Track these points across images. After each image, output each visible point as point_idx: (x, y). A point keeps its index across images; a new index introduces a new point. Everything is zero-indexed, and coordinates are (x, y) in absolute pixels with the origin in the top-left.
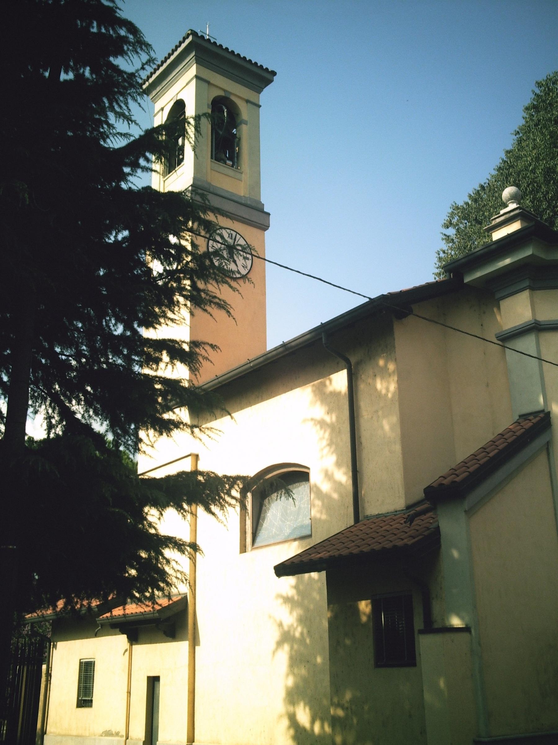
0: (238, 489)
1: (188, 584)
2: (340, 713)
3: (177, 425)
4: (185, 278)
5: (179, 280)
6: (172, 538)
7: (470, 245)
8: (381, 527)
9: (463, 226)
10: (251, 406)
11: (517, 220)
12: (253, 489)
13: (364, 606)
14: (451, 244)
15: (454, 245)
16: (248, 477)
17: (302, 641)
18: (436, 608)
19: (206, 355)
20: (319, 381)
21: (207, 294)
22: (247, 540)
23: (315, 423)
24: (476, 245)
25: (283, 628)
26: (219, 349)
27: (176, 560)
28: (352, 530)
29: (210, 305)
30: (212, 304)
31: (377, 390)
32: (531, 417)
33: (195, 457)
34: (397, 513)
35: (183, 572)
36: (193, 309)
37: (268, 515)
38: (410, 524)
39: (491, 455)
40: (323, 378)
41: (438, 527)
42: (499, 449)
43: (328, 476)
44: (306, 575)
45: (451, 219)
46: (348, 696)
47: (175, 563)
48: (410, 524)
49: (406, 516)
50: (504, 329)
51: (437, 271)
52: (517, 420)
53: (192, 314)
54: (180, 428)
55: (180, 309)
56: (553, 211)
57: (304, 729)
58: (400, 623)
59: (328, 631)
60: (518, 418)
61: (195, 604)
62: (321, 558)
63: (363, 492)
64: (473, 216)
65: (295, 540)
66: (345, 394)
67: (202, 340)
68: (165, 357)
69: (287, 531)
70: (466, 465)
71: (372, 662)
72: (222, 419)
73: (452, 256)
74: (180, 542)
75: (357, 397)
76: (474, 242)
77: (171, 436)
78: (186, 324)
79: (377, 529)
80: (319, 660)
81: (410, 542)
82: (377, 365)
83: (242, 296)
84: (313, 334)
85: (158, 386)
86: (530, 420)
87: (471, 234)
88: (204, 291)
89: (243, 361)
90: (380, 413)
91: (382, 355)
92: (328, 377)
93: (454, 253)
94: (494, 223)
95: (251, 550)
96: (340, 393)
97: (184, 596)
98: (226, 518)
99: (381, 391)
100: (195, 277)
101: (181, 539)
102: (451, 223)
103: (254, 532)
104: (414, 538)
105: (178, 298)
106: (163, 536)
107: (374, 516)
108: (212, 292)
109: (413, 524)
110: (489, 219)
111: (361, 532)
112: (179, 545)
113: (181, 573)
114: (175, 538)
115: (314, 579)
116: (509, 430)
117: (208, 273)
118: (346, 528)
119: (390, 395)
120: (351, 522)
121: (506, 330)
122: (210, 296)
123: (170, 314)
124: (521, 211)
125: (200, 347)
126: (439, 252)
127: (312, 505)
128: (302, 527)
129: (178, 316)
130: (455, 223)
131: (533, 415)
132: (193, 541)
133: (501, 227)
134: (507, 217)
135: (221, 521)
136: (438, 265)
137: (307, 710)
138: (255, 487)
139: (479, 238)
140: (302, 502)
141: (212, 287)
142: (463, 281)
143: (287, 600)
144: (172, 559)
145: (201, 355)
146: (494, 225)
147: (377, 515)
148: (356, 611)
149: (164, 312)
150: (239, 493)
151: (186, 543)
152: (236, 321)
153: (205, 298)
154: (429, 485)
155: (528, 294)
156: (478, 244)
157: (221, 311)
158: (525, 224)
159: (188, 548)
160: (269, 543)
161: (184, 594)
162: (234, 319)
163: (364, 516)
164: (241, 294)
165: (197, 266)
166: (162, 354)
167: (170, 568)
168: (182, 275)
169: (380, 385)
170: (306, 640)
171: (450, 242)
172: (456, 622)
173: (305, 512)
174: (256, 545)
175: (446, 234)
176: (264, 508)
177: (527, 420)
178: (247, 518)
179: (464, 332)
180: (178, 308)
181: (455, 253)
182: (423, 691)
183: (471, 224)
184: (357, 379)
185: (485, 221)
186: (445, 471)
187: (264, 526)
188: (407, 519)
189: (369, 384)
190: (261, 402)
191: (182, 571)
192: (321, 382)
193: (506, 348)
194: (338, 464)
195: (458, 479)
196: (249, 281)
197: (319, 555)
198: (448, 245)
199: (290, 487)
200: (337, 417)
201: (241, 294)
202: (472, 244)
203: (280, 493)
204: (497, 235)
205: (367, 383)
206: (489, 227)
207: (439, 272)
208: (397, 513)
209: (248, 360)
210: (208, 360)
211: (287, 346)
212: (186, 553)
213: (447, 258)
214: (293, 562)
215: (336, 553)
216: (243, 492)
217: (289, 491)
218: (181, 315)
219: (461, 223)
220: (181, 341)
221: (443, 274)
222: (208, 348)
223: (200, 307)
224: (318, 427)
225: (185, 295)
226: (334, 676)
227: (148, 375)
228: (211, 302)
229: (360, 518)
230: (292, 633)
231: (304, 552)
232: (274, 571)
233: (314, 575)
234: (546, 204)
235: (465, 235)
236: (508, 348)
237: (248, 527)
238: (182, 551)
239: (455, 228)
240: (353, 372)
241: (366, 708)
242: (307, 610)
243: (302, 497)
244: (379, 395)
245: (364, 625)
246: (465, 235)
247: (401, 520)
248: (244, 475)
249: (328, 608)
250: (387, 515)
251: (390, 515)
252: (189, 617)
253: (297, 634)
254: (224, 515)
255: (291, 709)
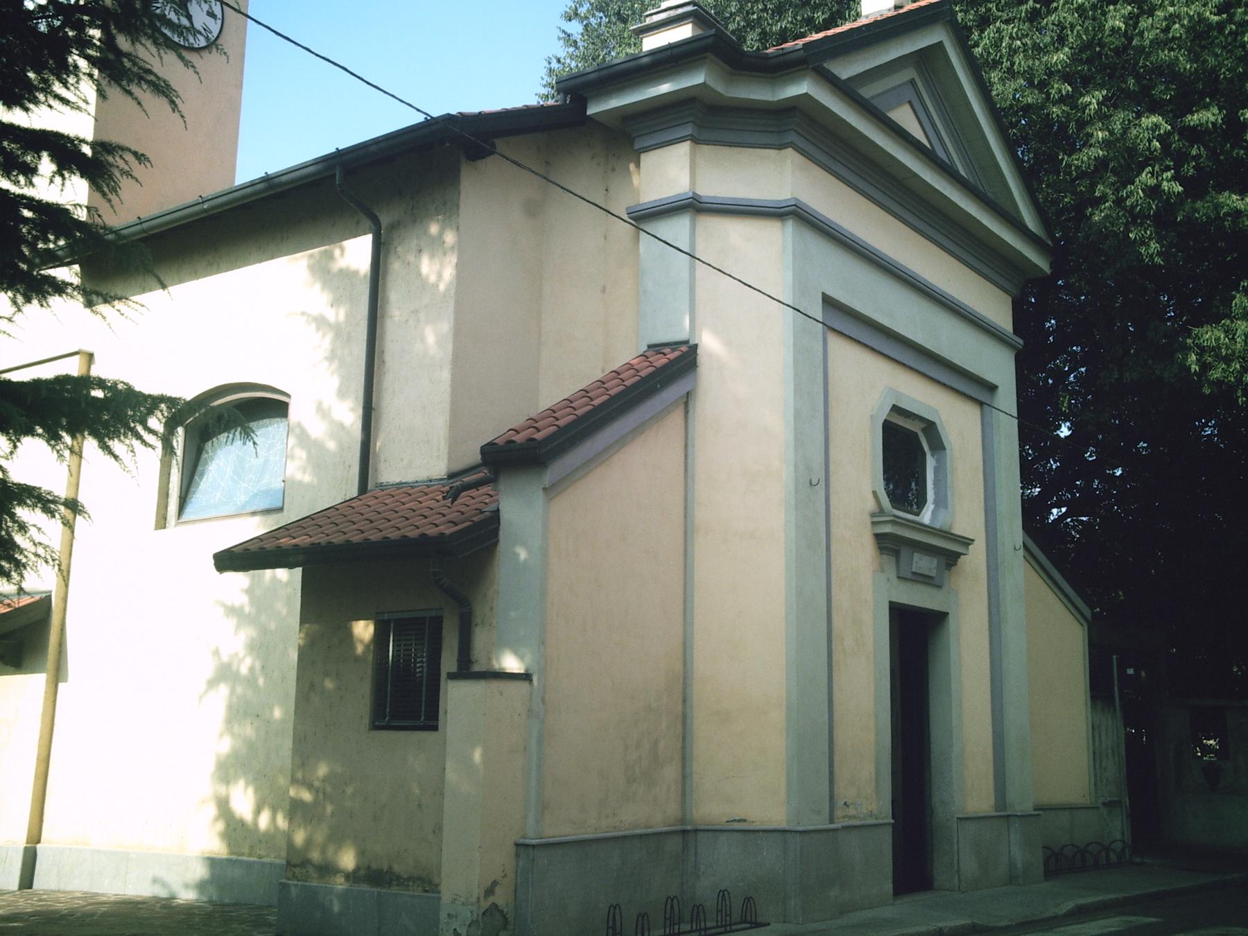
0: (161, 417)
1: (57, 567)
2: (307, 796)
3: (60, 288)
4: (92, 25)
5: (80, 27)
6: (34, 488)
7: (603, 56)
8: (404, 504)
9: (596, 22)
10: (198, 279)
11: (686, 22)
12: (188, 422)
13: (363, 630)
14: (571, 49)
15: (577, 51)
16: (180, 399)
17: (251, 681)
18: (480, 639)
19: (127, 168)
20: (322, 248)
21: (135, 64)
22: (169, 509)
23: (308, 320)
24: (612, 56)
25: (220, 658)
26: (149, 161)
27: (38, 526)
28: (353, 505)
29: (139, 84)
30: (143, 82)
31: (420, 275)
32: (667, 350)
33: (88, 358)
34: (432, 483)
35: (48, 546)
36: (106, 86)
37: (210, 468)
38: (452, 503)
39: (596, 402)
40: (329, 245)
41: (498, 510)
42: (610, 395)
43: (324, 413)
44: (268, 573)
45: (578, 6)
46: (322, 770)
47: (36, 530)
48: (452, 503)
49: (447, 488)
50: (641, 202)
51: (545, 91)
52: (644, 352)
53: (101, 94)
54: (67, 294)
55: (80, 82)
56: (744, 19)
57: (242, 823)
58: (419, 655)
59: (296, 667)
60: (645, 348)
61: (65, 610)
62: (296, 545)
63: (378, 444)
64: (615, 7)
65: (254, 513)
66: (365, 276)
67: (117, 143)
68: (46, 165)
69: (241, 498)
70: (554, 415)
71: (366, 721)
72: (143, 295)
73: (571, 69)
74: (48, 496)
75: (384, 284)
76: (610, 52)
77: (48, 305)
78: (89, 114)
79: (396, 506)
80: (277, 713)
81: (449, 530)
82: (426, 232)
83: (200, 77)
84: (320, 166)
85: (27, 213)
86: (665, 355)
87: (608, 38)
88: (128, 55)
89: (191, 198)
90: (422, 315)
91: (437, 217)
92: (339, 244)
93: (575, 65)
94: (649, 21)
95: (175, 526)
96: (356, 273)
97: (46, 597)
98: (137, 468)
99: (428, 276)
100: (113, 27)
101: (52, 492)
102: (576, 14)
103: (183, 496)
104: (456, 524)
105: (75, 58)
106: (15, 484)
107: (393, 485)
108: (144, 62)
109: (456, 502)
110: (640, 15)
111: (369, 509)
112: (44, 502)
113: (46, 547)
114: (40, 488)
115: (281, 582)
116: (629, 366)
117: (138, 23)
118: (344, 500)
119: (442, 287)
120: (354, 492)
121: (644, 203)
122: (140, 68)
123: (58, 88)
124: (696, 7)
125: (115, 153)
126: (551, 59)
127: (289, 456)
128: (267, 492)
129: (75, 94)
130: (583, 15)
131: (670, 347)
132: (71, 495)
133: (659, 31)
134: (672, 15)
135: (127, 469)
136: (547, 81)
137: (251, 791)
138: (192, 419)
139: (620, 46)
140: (271, 452)
141: (147, 53)
142: (586, 113)
143: (232, 611)
144: (30, 523)
145: (118, 167)
146: (648, 25)
147: (397, 484)
148: (348, 637)
149: (45, 81)
150: (162, 425)
151: (59, 498)
152: (185, 122)
153: (129, 69)
154: (490, 440)
155: (688, 147)
156: (617, 55)
157: (159, 97)
158: (699, 32)
159: (62, 508)
160: (208, 516)
161: (46, 593)
162: (182, 116)
163: (376, 484)
164: (198, 74)
165: (119, 5)
166: (40, 158)
167: (25, 539)
168: (86, 18)
169: (427, 266)
170: (257, 680)
171: (571, 45)
172: (511, 663)
173: (276, 469)
174: (185, 517)
175: (566, 31)
176: (204, 456)
177: (660, 353)
178: (174, 462)
179: (577, 195)
180: (75, 80)
181: (577, 66)
182: (445, 768)
183: (609, 20)
184: (388, 253)
185: (632, 18)
186: (518, 422)
187: (200, 488)
188: (448, 492)
189: (408, 263)
190: (216, 273)
191: (47, 544)
192: (325, 251)
193: (641, 231)
194: (342, 394)
195: (539, 436)
196: (217, 49)
197: (294, 541)
198: (567, 49)
199: (253, 425)
200: (348, 315)
201: (198, 74)
202: (606, 54)
203: (232, 432)
204: (652, 42)
205: (403, 262)
206: (639, 27)
207: (546, 93)
208: (432, 483)
209: (201, 196)
210: (130, 177)
211: (271, 181)
212: (57, 516)
213: (562, 72)
214: (246, 550)
215: (323, 540)
216: (171, 425)
217: (248, 429)
218: (81, 93)
219: (594, 16)
220: (77, 139)
221: (553, 97)
222: (129, 157)
223: (120, 85)
224: (313, 325)
225: (92, 56)
226: (300, 741)
227: (8, 191)
228: (141, 78)
229: (369, 488)
230: (235, 667)
231: (269, 534)
232: (213, 562)
233: (282, 574)
234: (736, 5)
235: (598, 37)
236: (645, 232)
237: (174, 487)
238: (51, 513)
239: (582, 22)
240: (382, 240)
241: (349, 790)
242: (264, 631)
243: (274, 443)
244: (423, 283)
245: (357, 659)
246: (598, 37)
247: (438, 495)
248: (174, 396)
249: (300, 630)
250: (416, 485)
251: (419, 486)
252: (52, 631)
253: (244, 670)
254: (133, 462)
255: (222, 790)
